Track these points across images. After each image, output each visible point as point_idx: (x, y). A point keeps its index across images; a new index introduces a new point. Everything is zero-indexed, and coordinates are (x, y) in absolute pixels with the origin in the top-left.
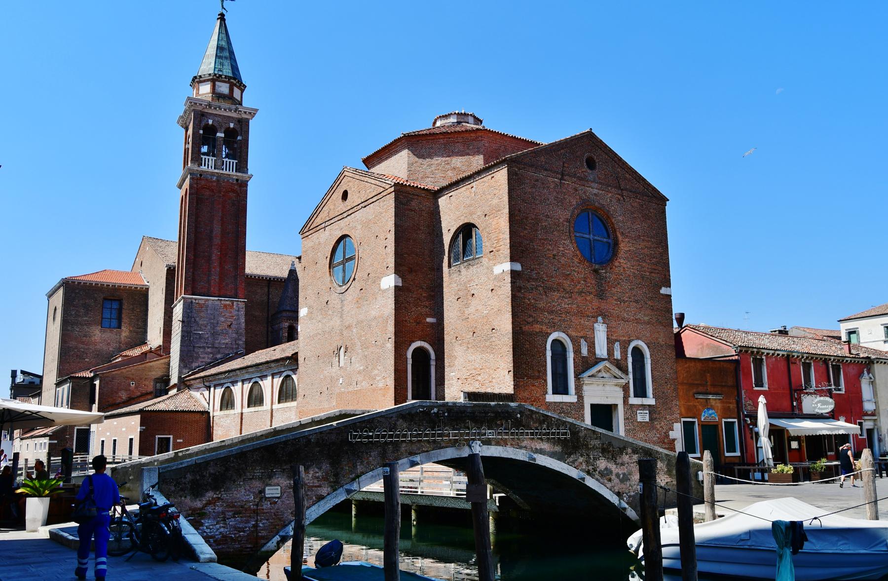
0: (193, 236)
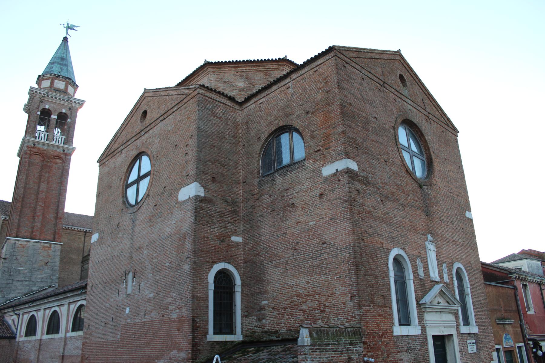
0: (22, 190)
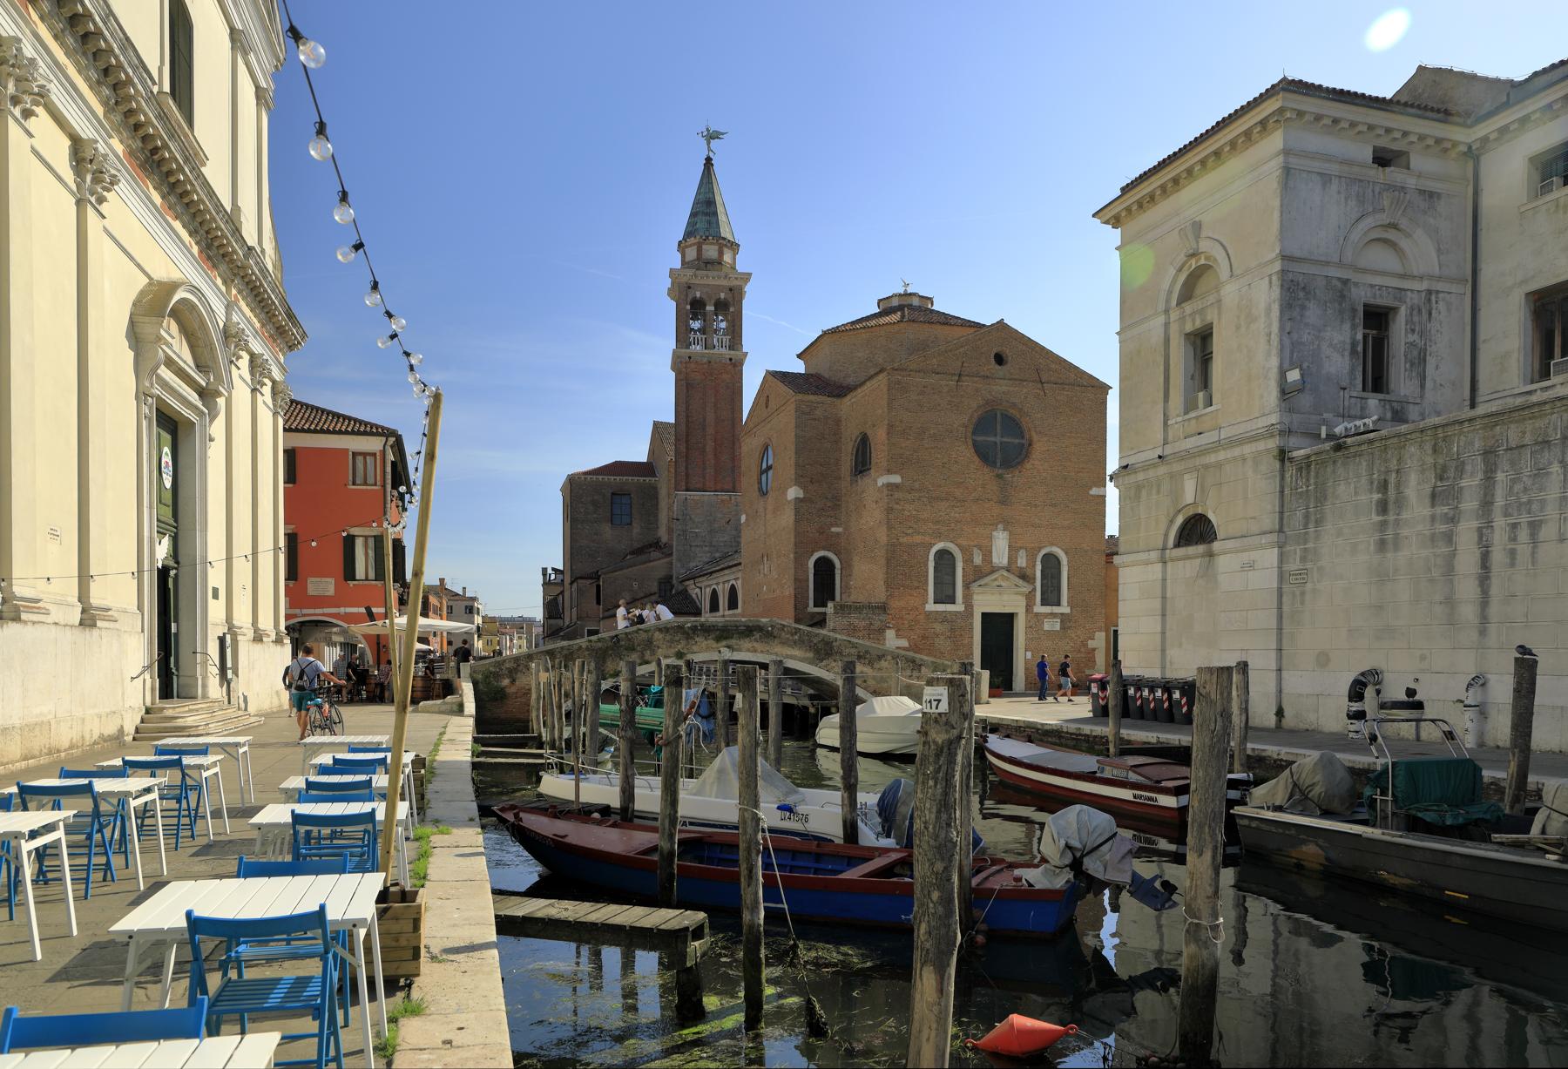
0: (683, 427)
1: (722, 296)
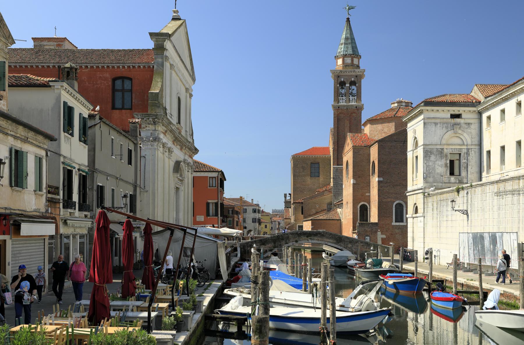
1: (353, 79)
